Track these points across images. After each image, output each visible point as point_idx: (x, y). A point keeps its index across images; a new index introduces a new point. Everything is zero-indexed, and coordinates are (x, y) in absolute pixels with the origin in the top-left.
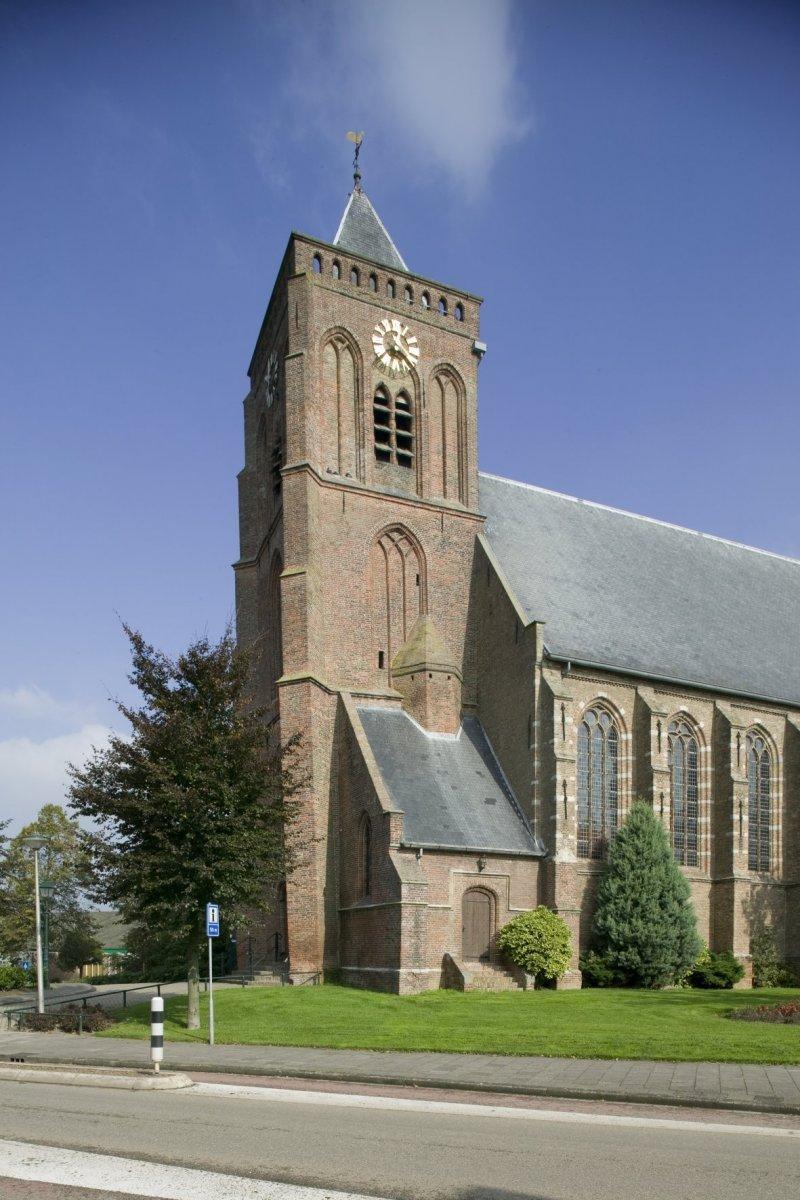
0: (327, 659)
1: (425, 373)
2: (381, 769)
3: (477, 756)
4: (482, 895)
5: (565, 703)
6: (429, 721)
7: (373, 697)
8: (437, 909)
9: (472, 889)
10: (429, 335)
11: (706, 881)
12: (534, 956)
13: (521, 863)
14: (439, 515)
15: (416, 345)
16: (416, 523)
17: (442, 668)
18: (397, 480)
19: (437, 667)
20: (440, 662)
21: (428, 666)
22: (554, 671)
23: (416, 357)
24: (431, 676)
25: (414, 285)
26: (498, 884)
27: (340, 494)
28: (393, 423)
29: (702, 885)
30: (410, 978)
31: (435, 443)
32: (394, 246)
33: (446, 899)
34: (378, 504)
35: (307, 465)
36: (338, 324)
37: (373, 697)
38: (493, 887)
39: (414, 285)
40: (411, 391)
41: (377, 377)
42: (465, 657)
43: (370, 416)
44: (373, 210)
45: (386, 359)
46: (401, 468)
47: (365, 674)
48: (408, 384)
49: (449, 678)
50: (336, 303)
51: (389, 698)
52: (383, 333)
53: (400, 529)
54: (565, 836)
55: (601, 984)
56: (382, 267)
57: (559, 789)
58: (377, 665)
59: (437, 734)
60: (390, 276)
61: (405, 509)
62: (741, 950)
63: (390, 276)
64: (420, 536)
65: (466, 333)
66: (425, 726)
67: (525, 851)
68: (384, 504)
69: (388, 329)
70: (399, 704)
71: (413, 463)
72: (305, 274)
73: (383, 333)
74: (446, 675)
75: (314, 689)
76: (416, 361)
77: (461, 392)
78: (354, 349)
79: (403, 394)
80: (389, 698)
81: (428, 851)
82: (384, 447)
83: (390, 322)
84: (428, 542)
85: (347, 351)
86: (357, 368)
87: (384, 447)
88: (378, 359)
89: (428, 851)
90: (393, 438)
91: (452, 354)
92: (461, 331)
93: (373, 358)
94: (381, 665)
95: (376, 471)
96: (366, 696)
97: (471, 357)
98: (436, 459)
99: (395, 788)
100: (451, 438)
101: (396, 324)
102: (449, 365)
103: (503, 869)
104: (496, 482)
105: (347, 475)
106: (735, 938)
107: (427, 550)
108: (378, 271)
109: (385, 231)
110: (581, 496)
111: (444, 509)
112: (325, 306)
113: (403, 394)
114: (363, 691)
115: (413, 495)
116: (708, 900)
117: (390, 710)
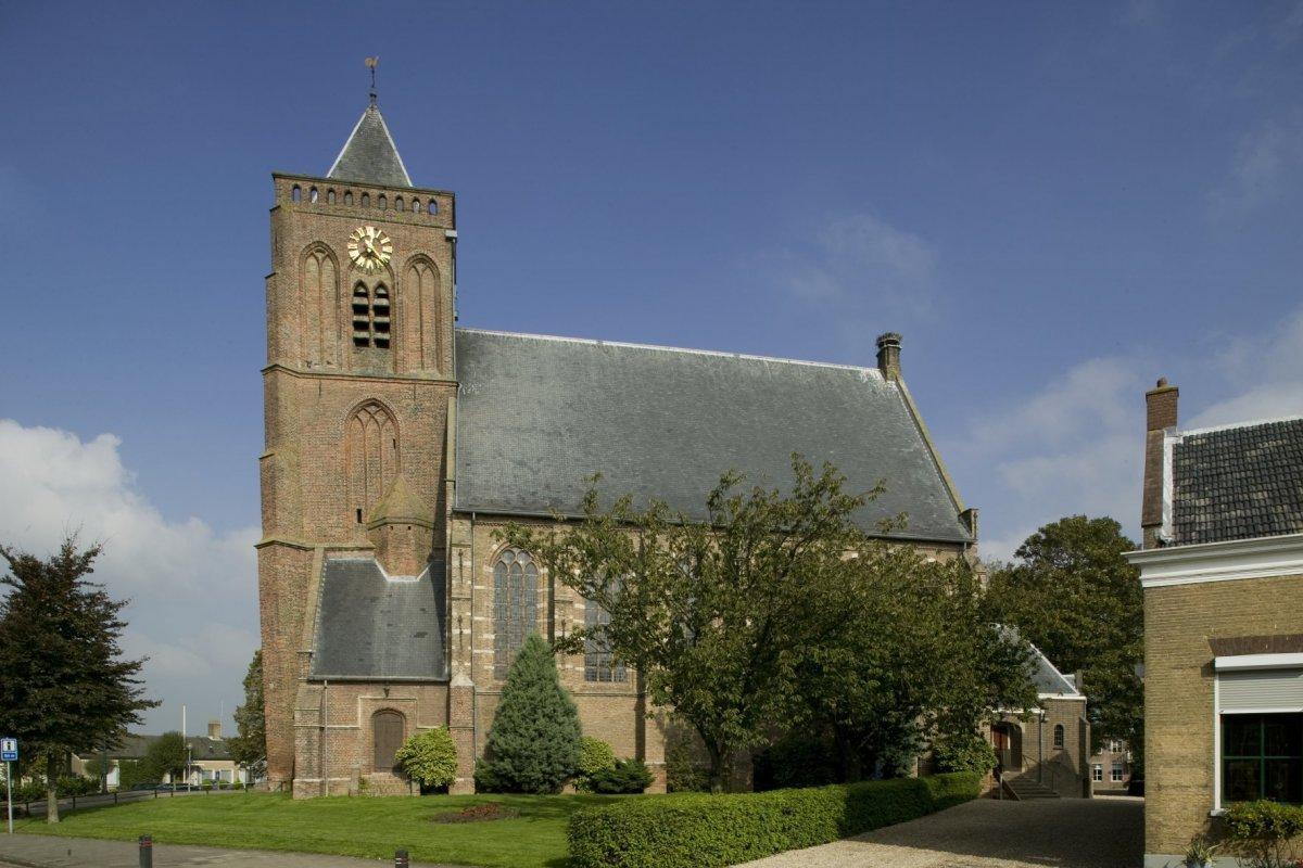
0: (305, 521)
1: (398, 265)
2: (325, 613)
3: (432, 595)
4: (387, 721)
5: (463, 550)
6: (391, 566)
7: (346, 549)
8: (346, 729)
9: (379, 713)
10: (402, 232)
11: (630, 696)
12: (415, 767)
13: (428, 688)
14: (412, 387)
15: (389, 244)
16: (390, 396)
17: (402, 520)
18: (375, 361)
19: (398, 520)
20: (400, 515)
21: (388, 520)
22: (464, 521)
23: (389, 254)
24: (409, 528)
25: (387, 193)
26: (405, 706)
27: (317, 382)
28: (372, 312)
29: (628, 699)
30: (303, 787)
31: (413, 323)
32: (396, 152)
33: (355, 720)
34: (352, 385)
35: (276, 365)
36: (317, 239)
37: (346, 549)
38: (401, 709)
39: (387, 193)
40: (388, 283)
41: (355, 277)
42: (437, 507)
43: (347, 310)
44: (383, 123)
45: (361, 261)
46: (379, 350)
47: (340, 530)
48: (385, 277)
49: (409, 528)
50: (314, 222)
51: (361, 549)
52: (357, 239)
53: (374, 403)
54: (461, 663)
55: (488, 790)
56: (355, 184)
57: (455, 623)
58: (356, 522)
59: (397, 577)
60: (363, 190)
61: (378, 386)
62: (655, 757)
63: (363, 190)
64: (393, 407)
65: (439, 224)
66: (387, 571)
67: (432, 678)
68: (358, 385)
69: (362, 235)
70: (372, 553)
71: (391, 344)
72: (279, 207)
73: (357, 239)
74: (407, 526)
75: (280, 550)
76: (389, 257)
77: (437, 275)
78: (332, 256)
79: (381, 285)
80: (361, 549)
81: (331, 682)
82: (363, 335)
83: (364, 228)
84: (401, 411)
85: (328, 259)
86: (337, 272)
87: (363, 335)
88: (354, 262)
89: (331, 682)
90: (371, 325)
91: (425, 245)
92: (434, 223)
93: (349, 262)
94: (360, 521)
95: (353, 356)
96: (340, 549)
97: (444, 243)
98: (413, 337)
99: (328, 629)
100: (428, 316)
101: (371, 231)
102: (423, 254)
103: (411, 693)
104: (508, 338)
105: (328, 363)
106: (647, 747)
107: (399, 417)
108: (352, 189)
109: (391, 141)
110: (600, 338)
111: (415, 381)
112: (304, 227)
113: (381, 285)
114: (338, 545)
115: (390, 371)
116: (634, 713)
117: (363, 559)
